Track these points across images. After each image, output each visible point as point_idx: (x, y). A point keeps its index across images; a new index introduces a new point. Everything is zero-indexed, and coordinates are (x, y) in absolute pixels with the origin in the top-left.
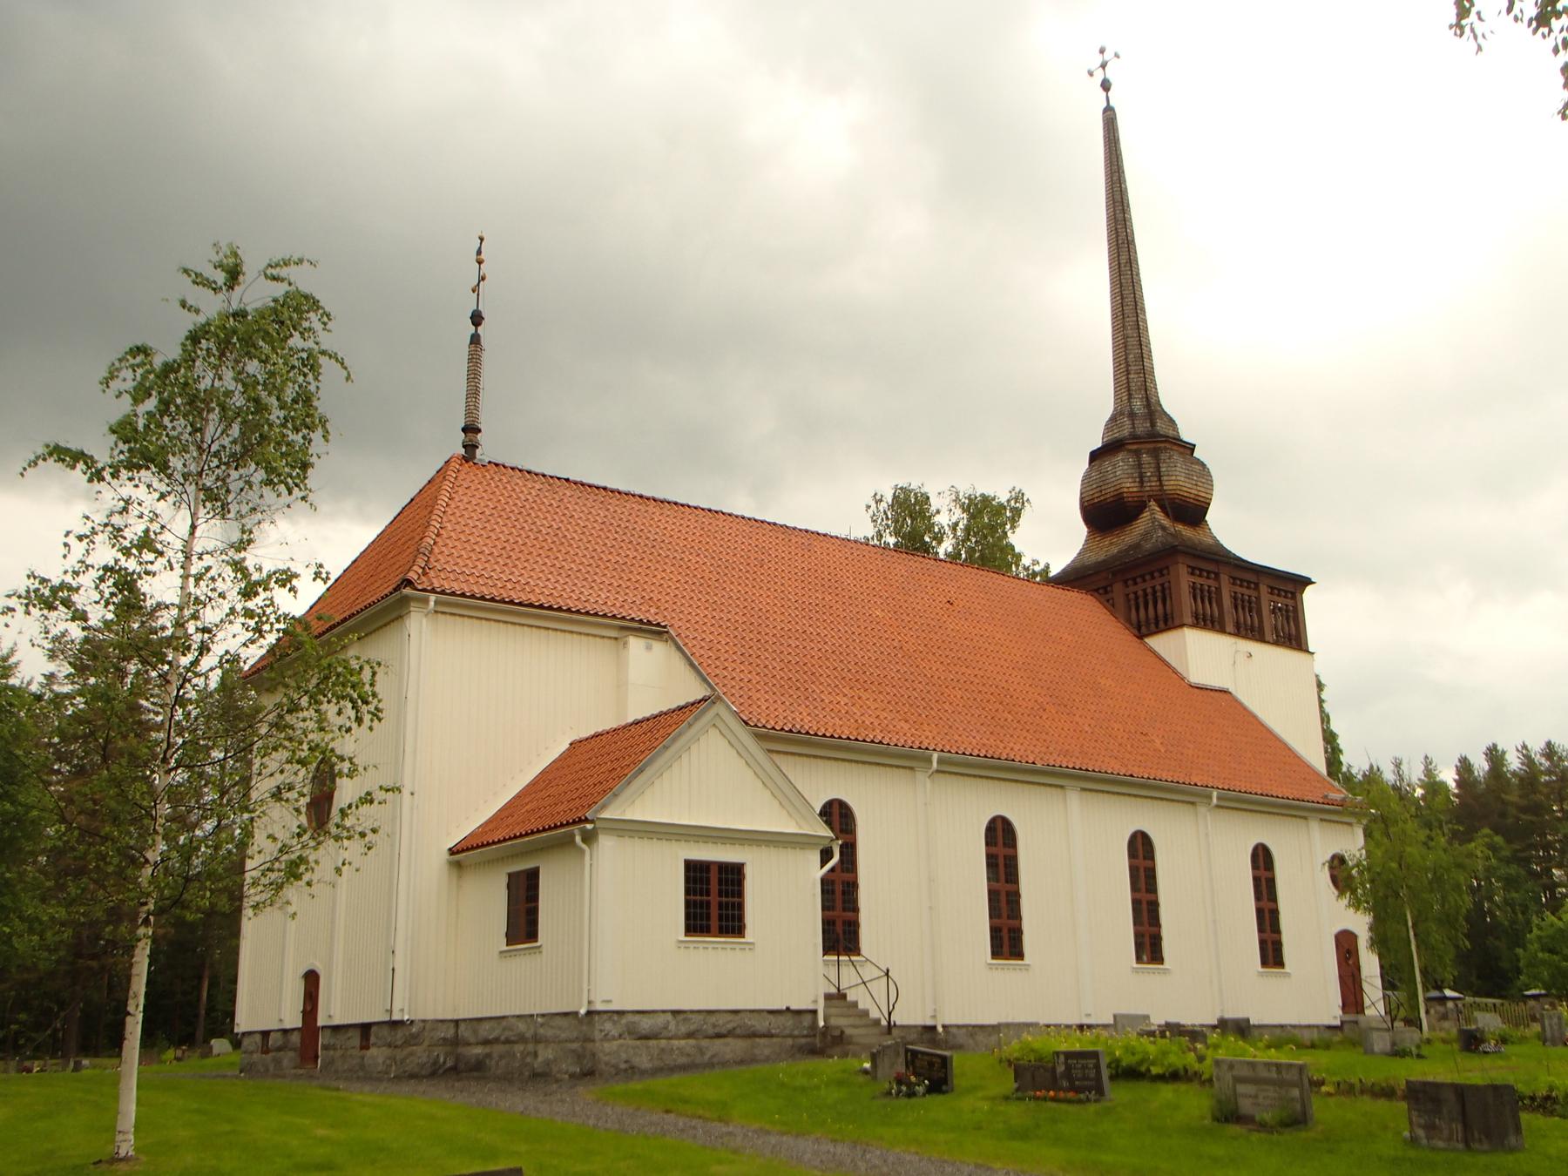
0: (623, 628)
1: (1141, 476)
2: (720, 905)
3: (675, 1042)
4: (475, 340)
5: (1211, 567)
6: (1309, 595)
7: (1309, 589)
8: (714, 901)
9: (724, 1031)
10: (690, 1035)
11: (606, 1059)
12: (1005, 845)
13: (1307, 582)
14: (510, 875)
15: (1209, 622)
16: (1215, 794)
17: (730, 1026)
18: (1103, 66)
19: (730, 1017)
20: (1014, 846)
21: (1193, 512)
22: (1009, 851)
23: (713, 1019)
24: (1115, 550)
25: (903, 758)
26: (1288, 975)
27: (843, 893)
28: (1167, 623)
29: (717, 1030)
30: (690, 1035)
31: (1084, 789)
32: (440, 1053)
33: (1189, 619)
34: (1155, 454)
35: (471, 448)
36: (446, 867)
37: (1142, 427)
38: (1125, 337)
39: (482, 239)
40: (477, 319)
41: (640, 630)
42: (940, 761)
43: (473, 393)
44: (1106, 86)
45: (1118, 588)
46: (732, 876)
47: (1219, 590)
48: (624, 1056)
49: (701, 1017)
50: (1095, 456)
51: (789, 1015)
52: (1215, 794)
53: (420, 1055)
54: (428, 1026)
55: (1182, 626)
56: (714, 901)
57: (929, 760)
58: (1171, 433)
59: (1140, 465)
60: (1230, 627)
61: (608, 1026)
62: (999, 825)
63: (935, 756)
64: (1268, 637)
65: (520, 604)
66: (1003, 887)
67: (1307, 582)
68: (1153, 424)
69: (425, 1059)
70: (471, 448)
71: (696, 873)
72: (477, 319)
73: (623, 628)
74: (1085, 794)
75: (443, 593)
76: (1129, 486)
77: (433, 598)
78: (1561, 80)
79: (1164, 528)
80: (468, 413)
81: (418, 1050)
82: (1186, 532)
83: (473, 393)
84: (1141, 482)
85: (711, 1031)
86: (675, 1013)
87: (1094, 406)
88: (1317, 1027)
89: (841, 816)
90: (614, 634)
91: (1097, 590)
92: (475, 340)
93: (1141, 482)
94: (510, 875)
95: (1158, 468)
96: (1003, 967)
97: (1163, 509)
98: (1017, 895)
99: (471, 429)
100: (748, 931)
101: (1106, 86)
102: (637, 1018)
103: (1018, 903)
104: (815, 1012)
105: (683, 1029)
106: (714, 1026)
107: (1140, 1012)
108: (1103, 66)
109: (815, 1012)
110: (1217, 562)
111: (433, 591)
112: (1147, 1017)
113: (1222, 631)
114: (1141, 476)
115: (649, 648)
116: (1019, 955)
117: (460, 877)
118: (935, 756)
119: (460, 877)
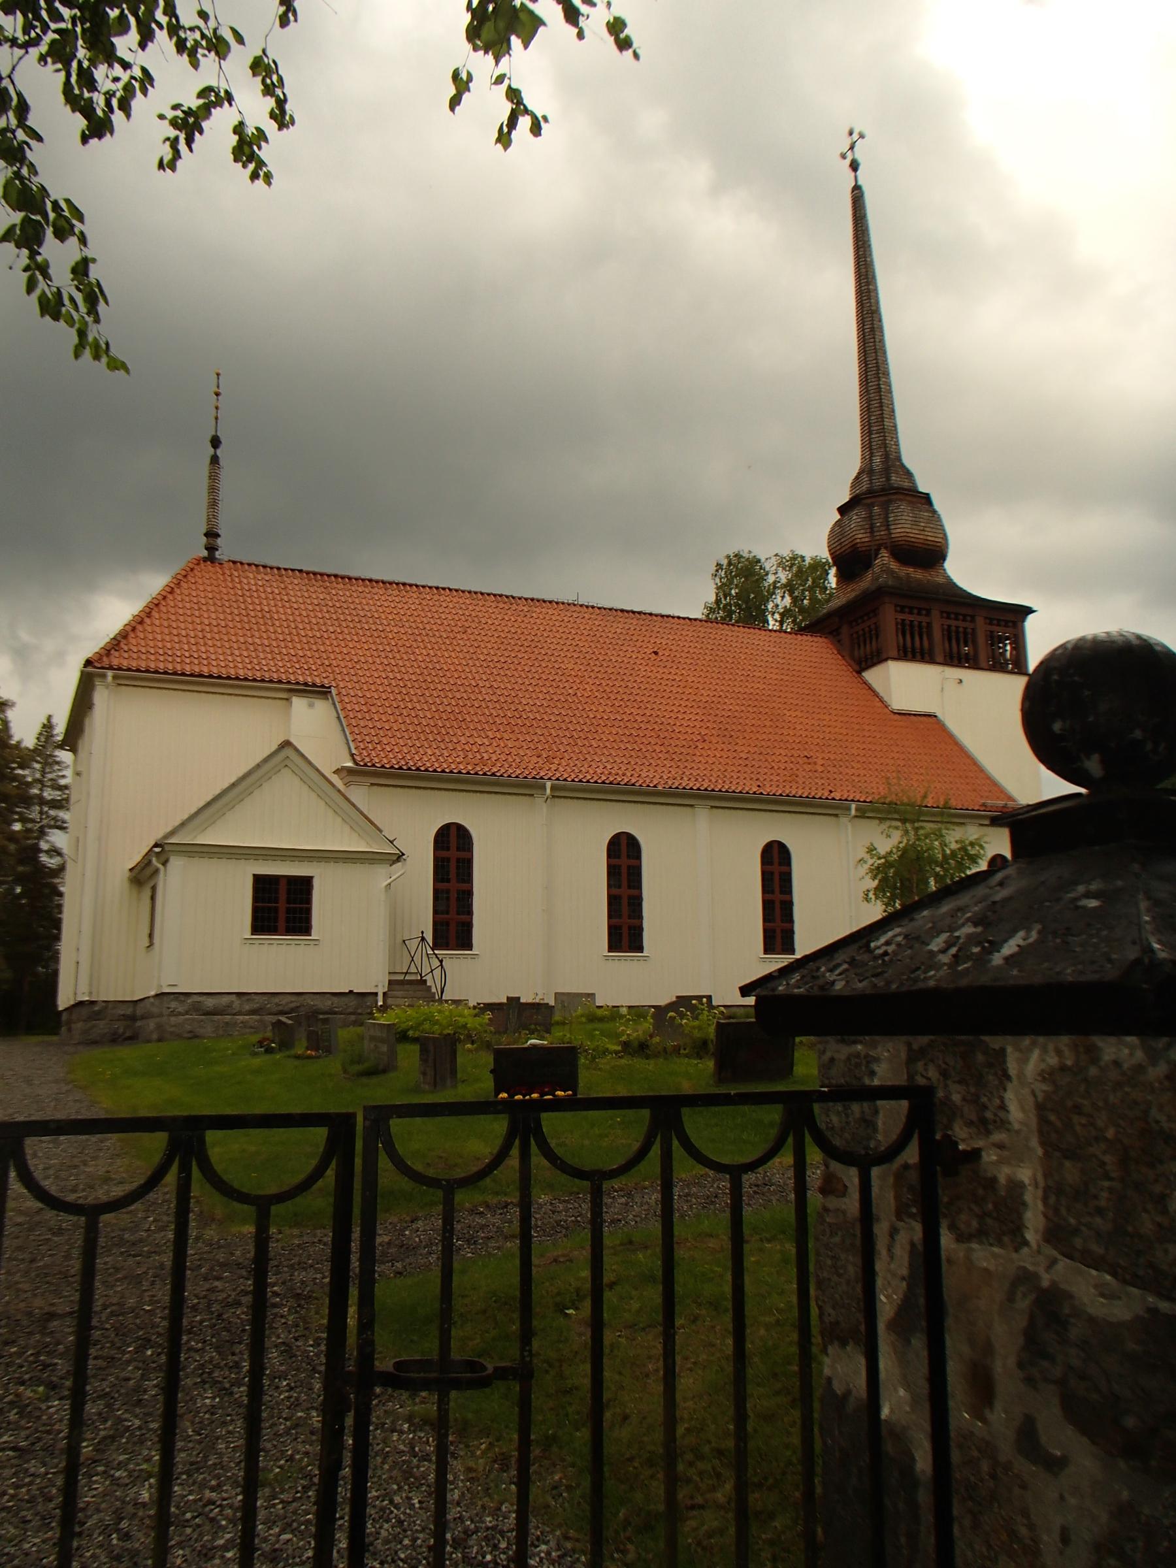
0: (290, 690)
1: (872, 527)
2: (288, 911)
3: (241, 1017)
4: (215, 460)
7: (1030, 617)
8: (282, 906)
9: (286, 1009)
10: (253, 1012)
11: (172, 1029)
12: (780, 864)
13: (1029, 611)
14: (259, 880)
15: (909, 654)
16: (853, 806)
17: (293, 1005)
18: (852, 148)
19: (293, 998)
20: (789, 864)
21: (934, 554)
22: (633, 862)
23: (276, 1000)
24: (853, 594)
25: (524, 787)
27: (458, 899)
28: (875, 659)
29: (280, 1008)
30: (253, 1012)
31: (712, 807)
32: (120, 1027)
33: (894, 653)
34: (885, 508)
35: (211, 549)
36: (126, 884)
37: (878, 482)
38: (869, 401)
39: (218, 375)
40: (216, 442)
41: (310, 692)
42: (553, 788)
43: (213, 504)
44: (854, 166)
45: (845, 630)
46: (302, 888)
47: (929, 625)
48: (188, 1027)
49: (265, 998)
50: (842, 510)
51: (352, 997)
52: (853, 806)
53: (102, 1027)
54: (110, 1006)
55: (886, 660)
56: (282, 906)
57: (544, 787)
58: (906, 484)
59: (870, 517)
60: (940, 659)
61: (173, 1005)
62: (624, 841)
63: (549, 784)
64: (983, 665)
65: (192, 675)
66: (625, 892)
67: (1029, 611)
68: (888, 479)
69: (106, 1031)
70: (211, 549)
71: (263, 885)
72: (216, 442)
73: (290, 690)
74: (715, 811)
75: (120, 669)
76: (862, 537)
77: (110, 673)
78: (68, 107)
79: (892, 572)
80: (209, 520)
81: (101, 1024)
82: (917, 574)
83: (213, 504)
84: (872, 532)
85: (275, 1009)
86: (239, 995)
87: (841, 464)
89: (458, 836)
90: (284, 695)
91: (831, 633)
92: (215, 460)
94: (259, 880)
95: (887, 517)
96: (619, 959)
98: (791, 903)
99: (211, 534)
100: (313, 931)
101: (854, 166)
103: (640, 905)
104: (376, 994)
105: (247, 1007)
106: (277, 1005)
108: (852, 148)
109: (376, 994)
111: (111, 668)
112: (591, 996)
114: (872, 527)
116: (640, 949)
117: (139, 892)
118: (549, 784)
119: (139, 892)
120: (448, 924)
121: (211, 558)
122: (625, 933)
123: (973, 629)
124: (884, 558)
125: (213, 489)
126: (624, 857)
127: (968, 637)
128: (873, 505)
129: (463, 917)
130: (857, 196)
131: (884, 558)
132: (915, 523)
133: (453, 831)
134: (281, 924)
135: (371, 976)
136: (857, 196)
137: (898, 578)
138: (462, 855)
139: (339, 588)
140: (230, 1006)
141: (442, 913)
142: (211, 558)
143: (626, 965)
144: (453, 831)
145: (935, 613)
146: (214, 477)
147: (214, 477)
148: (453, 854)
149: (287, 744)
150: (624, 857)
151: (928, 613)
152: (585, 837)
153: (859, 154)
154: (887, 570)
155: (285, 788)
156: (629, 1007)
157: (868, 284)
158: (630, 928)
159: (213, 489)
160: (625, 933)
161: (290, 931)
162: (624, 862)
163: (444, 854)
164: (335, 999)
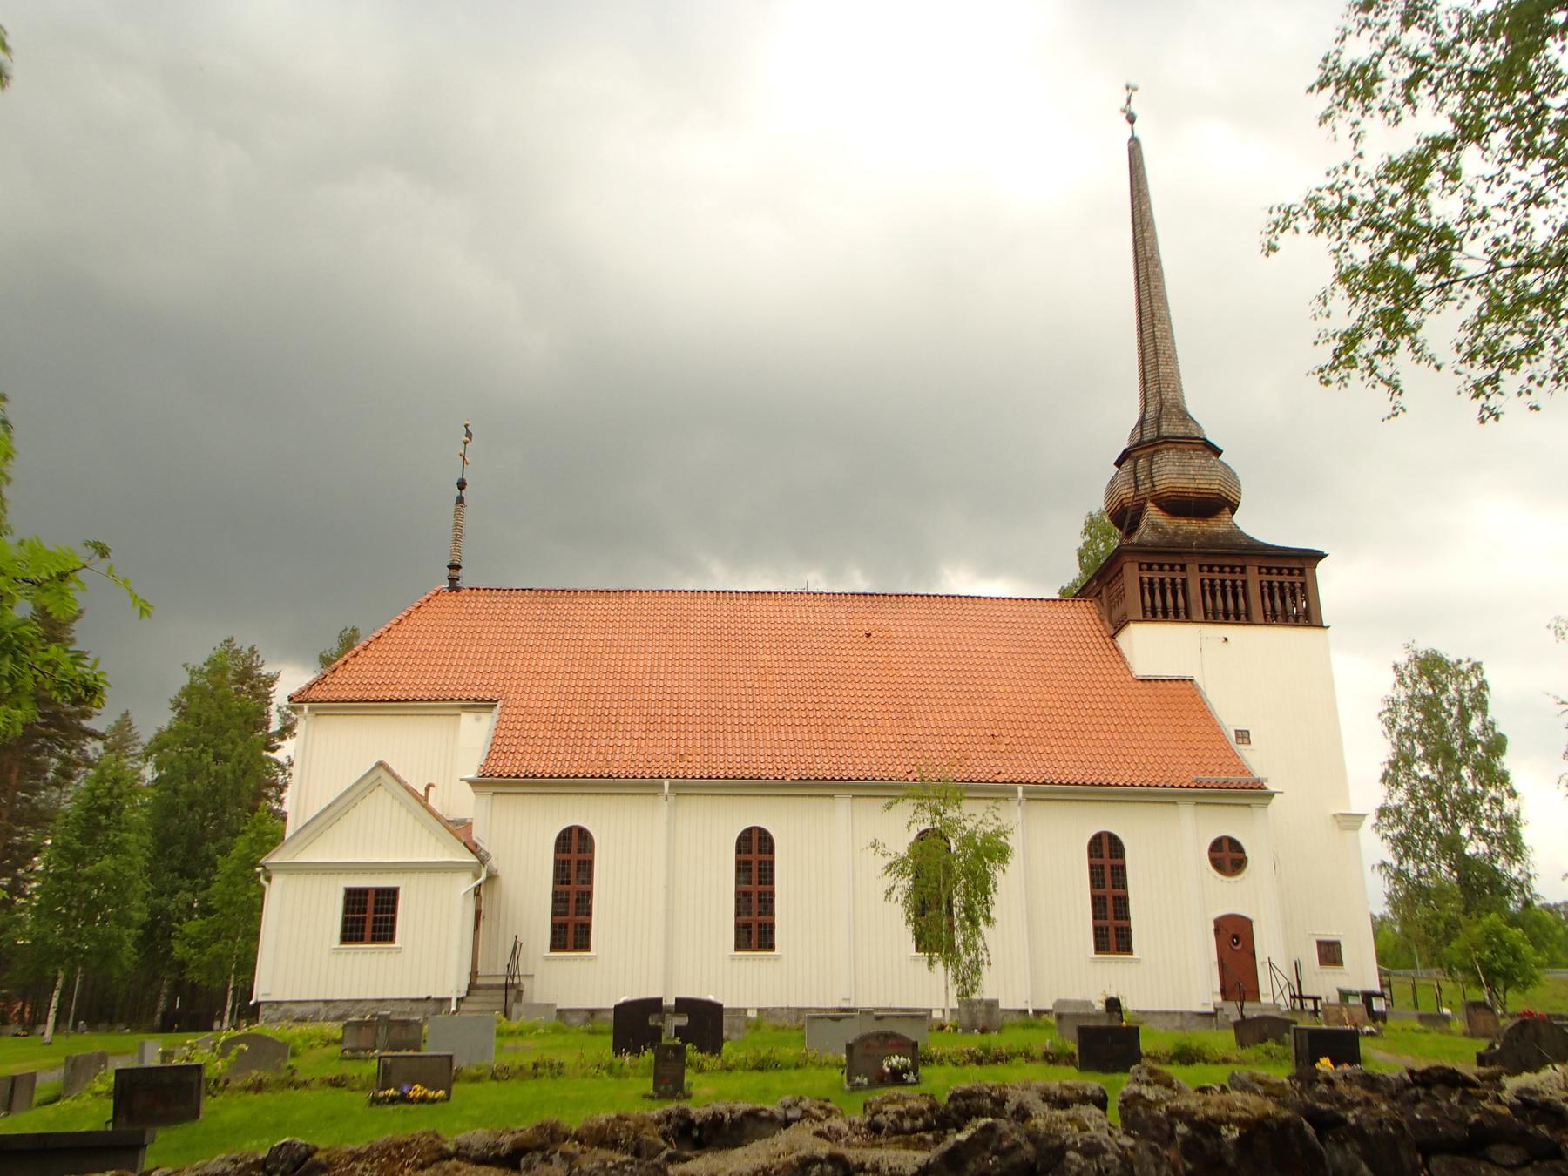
0: (463, 707)
2: (375, 920)
4: (460, 500)
5: (1179, 560)
6: (1324, 573)
7: (1321, 566)
13: (1318, 556)
14: (350, 893)
15: (1154, 614)
21: (1220, 504)
25: (641, 785)
26: (1138, 961)
40: (462, 485)
46: (387, 899)
47: (1184, 581)
52: (1020, 788)
56: (370, 916)
60: (1197, 612)
62: (755, 837)
63: (666, 783)
67: (1318, 556)
70: (452, 580)
72: (462, 485)
77: (306, 706)
84: (1136, 487)
86: (327, 1002)
87: (1121, 417)
88: (1182, 1013)
92: (460, 500)
93: (1136, 487)
94: (350, 893)
97: (1158, 505)
102: (293, 1007)
105: (332, 1014)
107: (741, 1006)
110: (1179, 554)
113: (1188, 619)
115: (478, 719)
116: (771, 947)
120: (566, 926)
121: (454, 587)
122: (755, 928)
123: (1244, 582)
124: (1153, 514)
125: (458, 527)
126: (755, 855)
127: (1238, 591)
128: (1139, 457)
129: (582, 918)
130: (1134, 147)
131: (1153, 514)
132: (1182, 472)
133: (575, 834)
134: (768, 887)
135: (450, 982)
136: (1134, 147)
137: (1164, 533)
138: (583, 856)
139: (562, 605)
140: (316, 1013)
141: (561, 914)
142: (454, 587)
143: (755, 962)
144: (575, 834)
145: (1192, 569)
146: (458, 516)
147: (458, 516)
148: (574, 856)
149: (380, 764)
150: (755, 855)
151: (1183, 568)
152: (709, 837)
153: (1134, 108)
154: (1154, 527)
155: (382, 804)
156: (759, 1010)
157: (1143, 232)
158: (760, 926)
159: (458, 527)
160: (755, 928)
161: (374, 939)
162: (755, 857)
163: (565, 856)
164: (414, 1005)
